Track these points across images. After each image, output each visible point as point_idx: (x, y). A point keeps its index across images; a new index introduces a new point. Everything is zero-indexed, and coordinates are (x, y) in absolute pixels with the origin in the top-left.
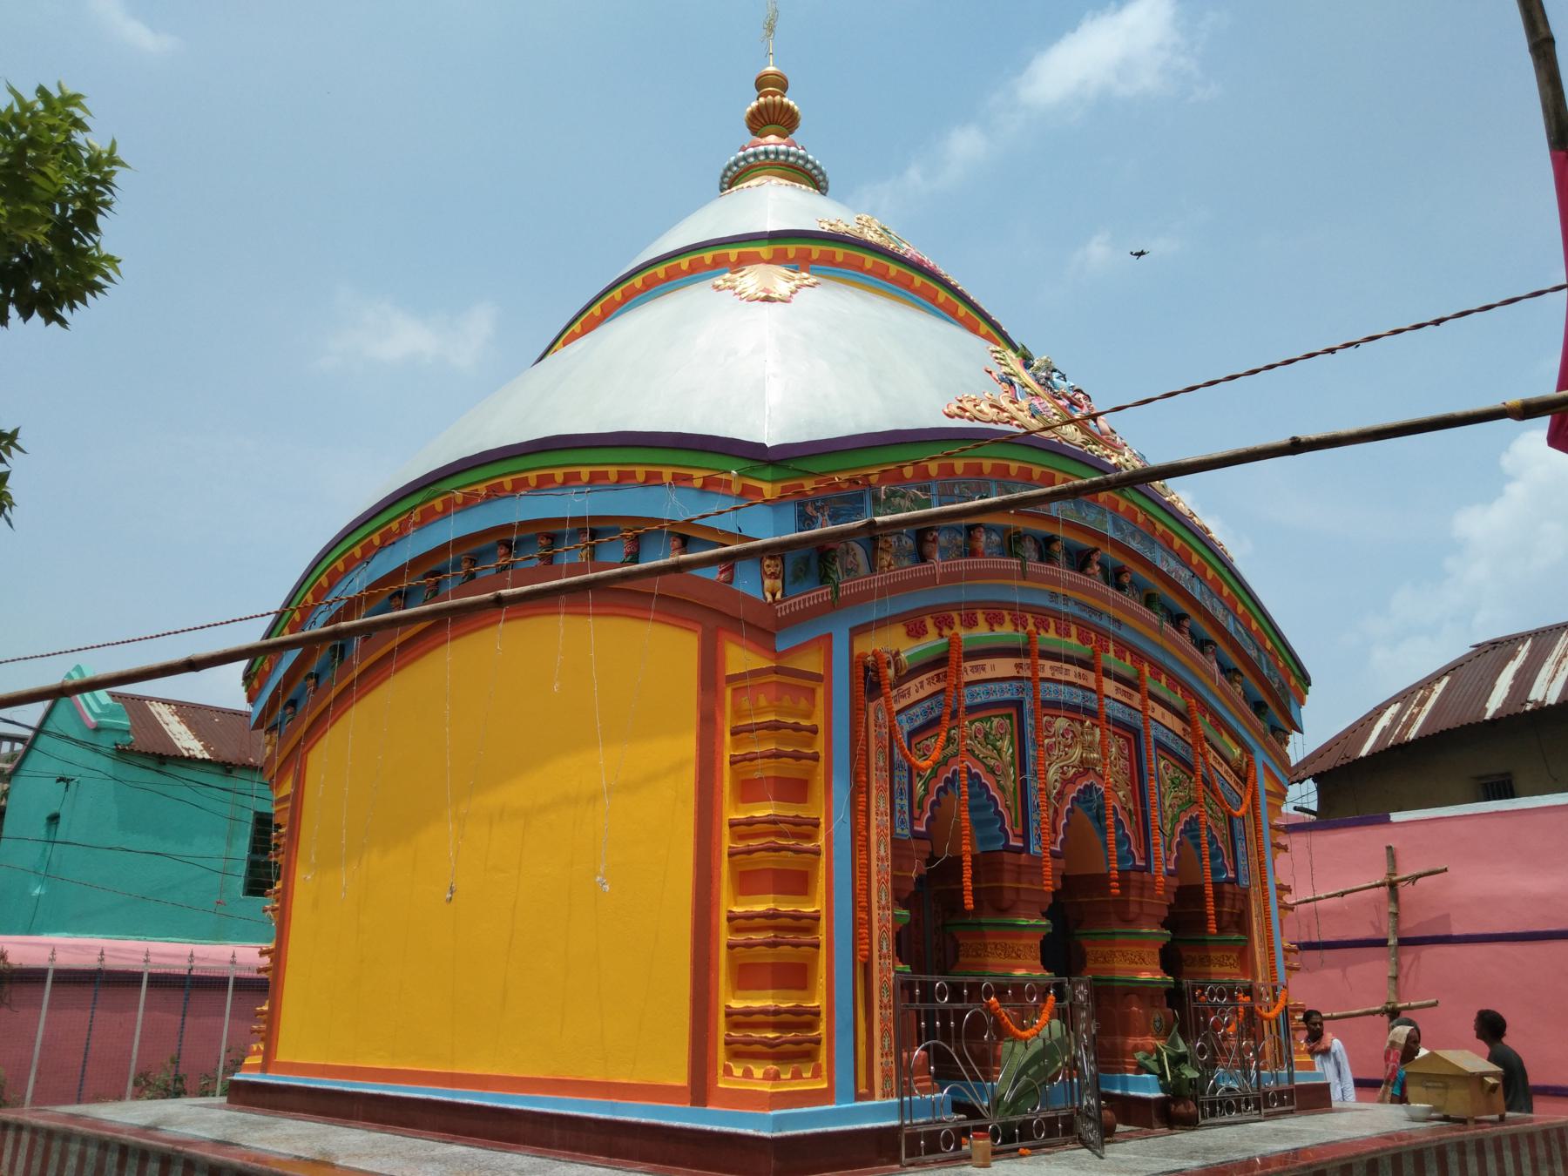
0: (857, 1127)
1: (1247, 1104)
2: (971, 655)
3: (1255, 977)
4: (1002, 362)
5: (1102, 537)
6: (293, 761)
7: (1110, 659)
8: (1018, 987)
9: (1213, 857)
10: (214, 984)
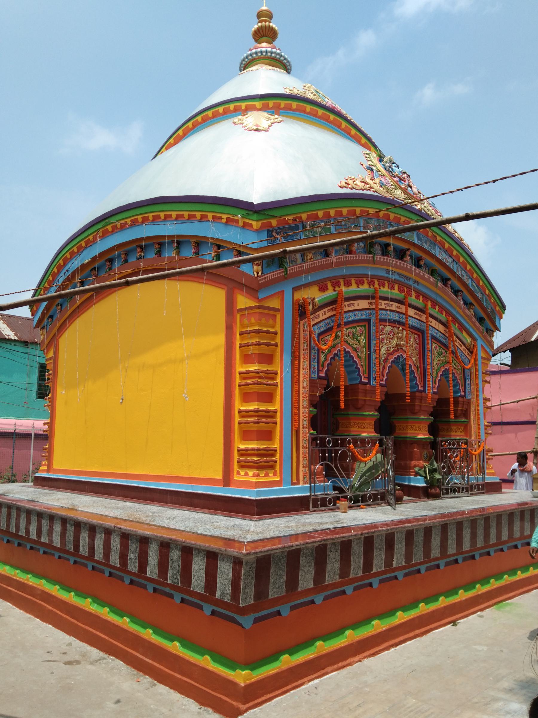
0: (292, 496)
1: (463, 489)
2: (348, 299)
3: (471, 437)
4: (368, 159)
5: (411, 243)
6: (53, 342)
7: (412, 299)
8: (363, 441)
9: (454, 386)
10: (26, 436)
